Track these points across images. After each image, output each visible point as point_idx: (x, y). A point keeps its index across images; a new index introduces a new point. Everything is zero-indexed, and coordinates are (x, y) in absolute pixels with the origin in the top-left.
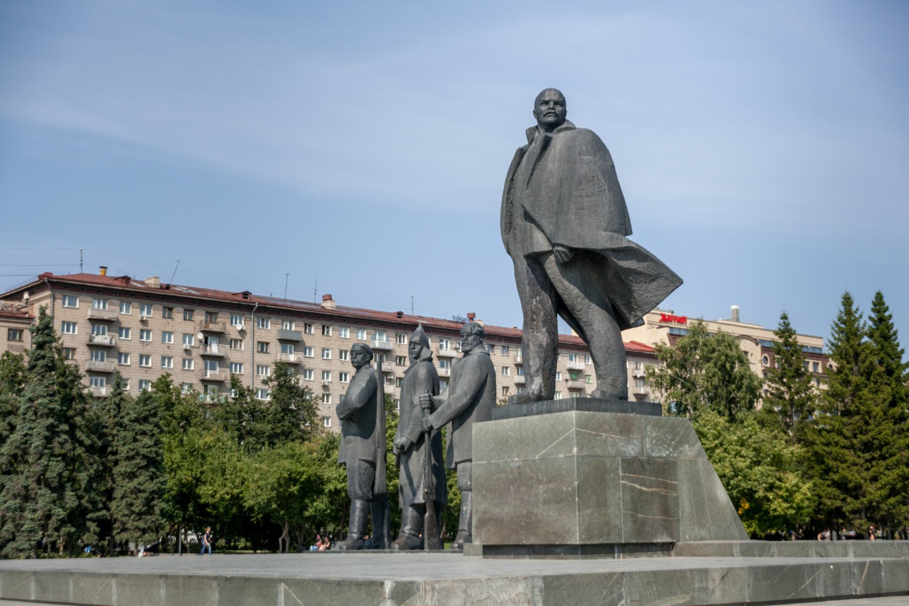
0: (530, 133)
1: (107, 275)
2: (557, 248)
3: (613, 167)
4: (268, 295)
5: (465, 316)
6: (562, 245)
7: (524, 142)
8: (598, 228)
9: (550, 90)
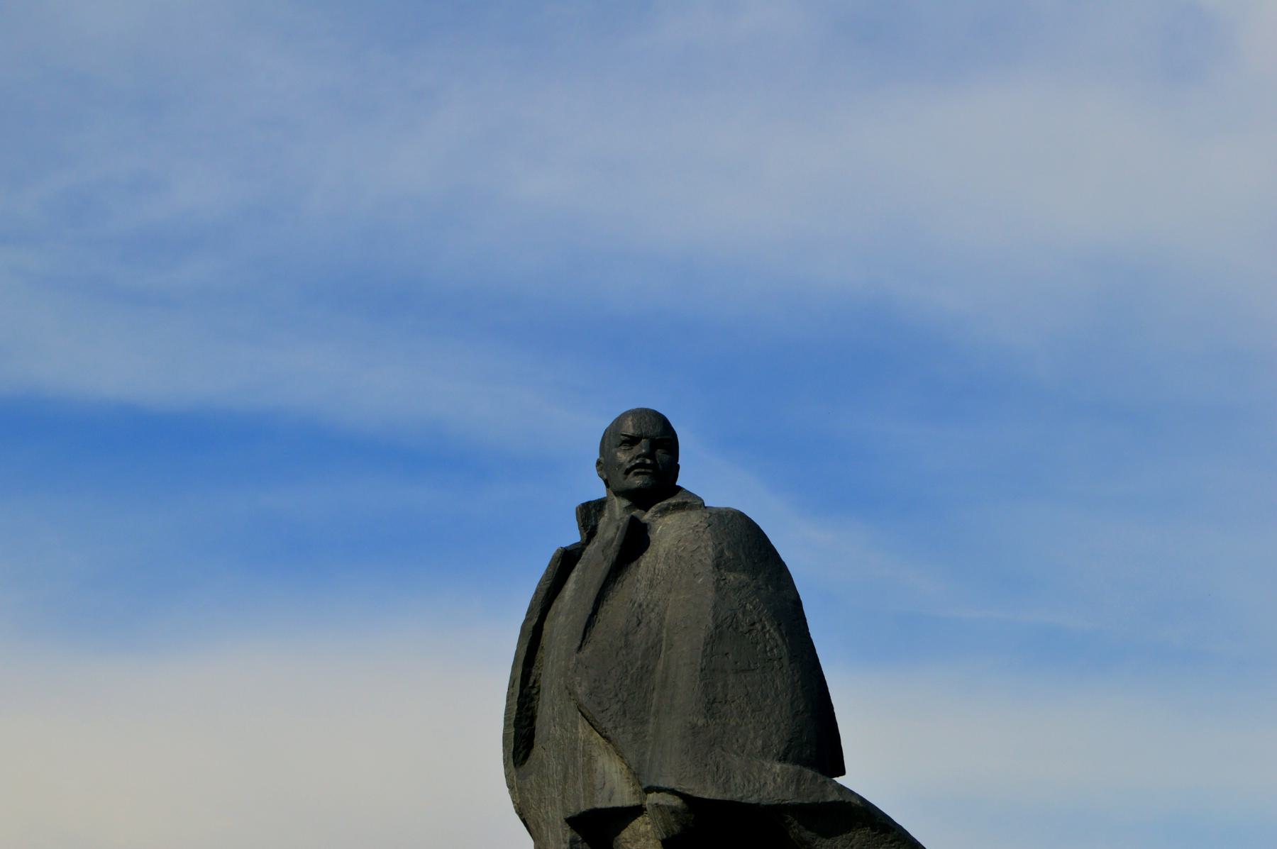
0: (589, 514)
2: (653, 798)
3: (798, 603)
6: (672, 792)
7: (573, 536)
8: (765, 751)
9: (625, 415)
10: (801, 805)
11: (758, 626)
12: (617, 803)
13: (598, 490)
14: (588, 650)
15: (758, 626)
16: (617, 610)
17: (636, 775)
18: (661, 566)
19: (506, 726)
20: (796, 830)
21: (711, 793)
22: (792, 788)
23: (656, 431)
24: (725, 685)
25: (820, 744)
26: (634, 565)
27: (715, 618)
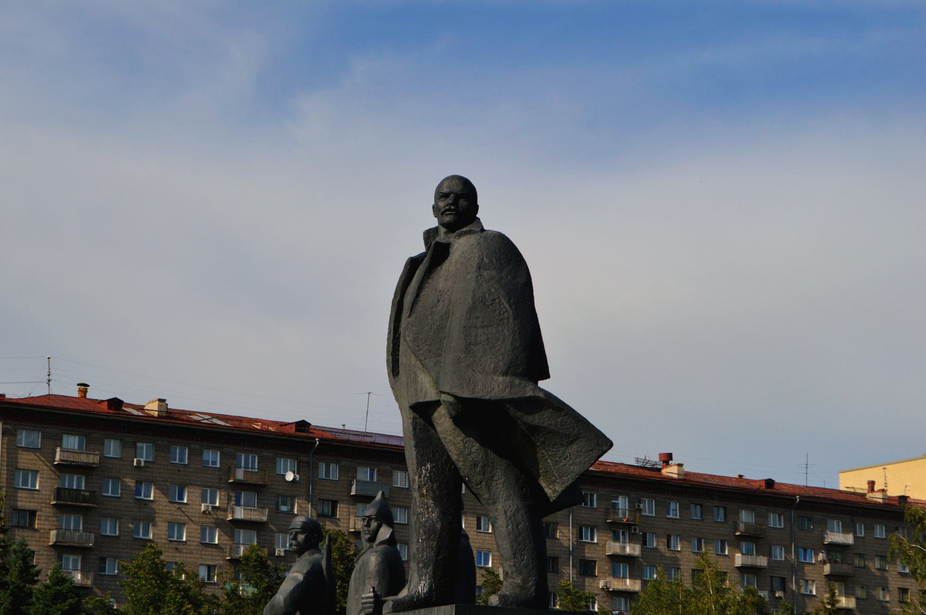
1: (88, 396)
4: (338, 425)
5: (655, 458)
6: (448, 394)
8: (495, 371)
10: (512, 399)
11: (497, 301)
12: (429, 399)
13: (434, 223)
14: (414, 316)
15: (497, 301)
16: (428, 295)
17: (436, 383)
18: (452, 268)
19: (388, 355)
20: (513, 412)
21: (466, 395)
22: (508, 390)
23: (457, 188)
24: (476, 336)
25: (534, 362)
26: (439, 268)
27: (473, 298)
